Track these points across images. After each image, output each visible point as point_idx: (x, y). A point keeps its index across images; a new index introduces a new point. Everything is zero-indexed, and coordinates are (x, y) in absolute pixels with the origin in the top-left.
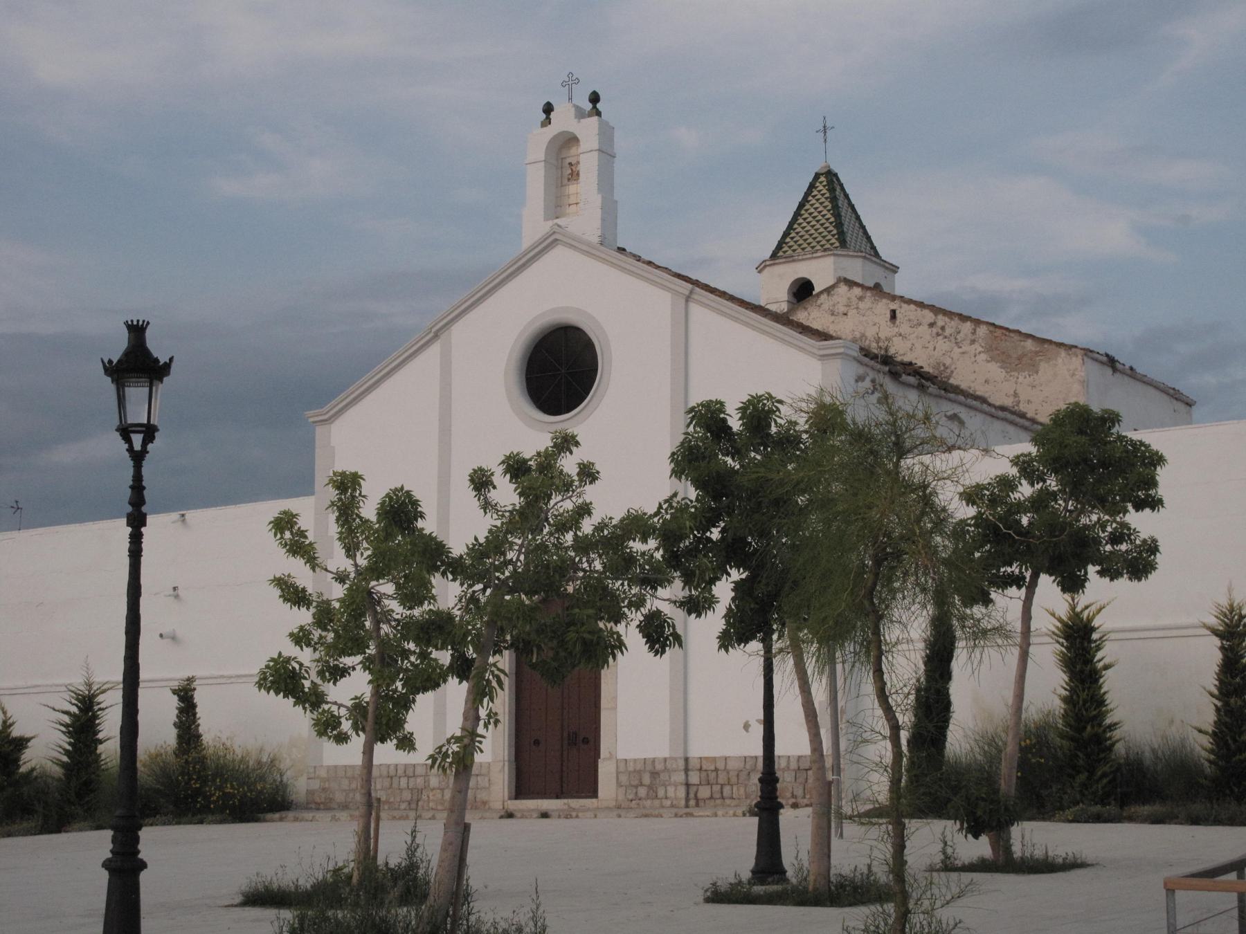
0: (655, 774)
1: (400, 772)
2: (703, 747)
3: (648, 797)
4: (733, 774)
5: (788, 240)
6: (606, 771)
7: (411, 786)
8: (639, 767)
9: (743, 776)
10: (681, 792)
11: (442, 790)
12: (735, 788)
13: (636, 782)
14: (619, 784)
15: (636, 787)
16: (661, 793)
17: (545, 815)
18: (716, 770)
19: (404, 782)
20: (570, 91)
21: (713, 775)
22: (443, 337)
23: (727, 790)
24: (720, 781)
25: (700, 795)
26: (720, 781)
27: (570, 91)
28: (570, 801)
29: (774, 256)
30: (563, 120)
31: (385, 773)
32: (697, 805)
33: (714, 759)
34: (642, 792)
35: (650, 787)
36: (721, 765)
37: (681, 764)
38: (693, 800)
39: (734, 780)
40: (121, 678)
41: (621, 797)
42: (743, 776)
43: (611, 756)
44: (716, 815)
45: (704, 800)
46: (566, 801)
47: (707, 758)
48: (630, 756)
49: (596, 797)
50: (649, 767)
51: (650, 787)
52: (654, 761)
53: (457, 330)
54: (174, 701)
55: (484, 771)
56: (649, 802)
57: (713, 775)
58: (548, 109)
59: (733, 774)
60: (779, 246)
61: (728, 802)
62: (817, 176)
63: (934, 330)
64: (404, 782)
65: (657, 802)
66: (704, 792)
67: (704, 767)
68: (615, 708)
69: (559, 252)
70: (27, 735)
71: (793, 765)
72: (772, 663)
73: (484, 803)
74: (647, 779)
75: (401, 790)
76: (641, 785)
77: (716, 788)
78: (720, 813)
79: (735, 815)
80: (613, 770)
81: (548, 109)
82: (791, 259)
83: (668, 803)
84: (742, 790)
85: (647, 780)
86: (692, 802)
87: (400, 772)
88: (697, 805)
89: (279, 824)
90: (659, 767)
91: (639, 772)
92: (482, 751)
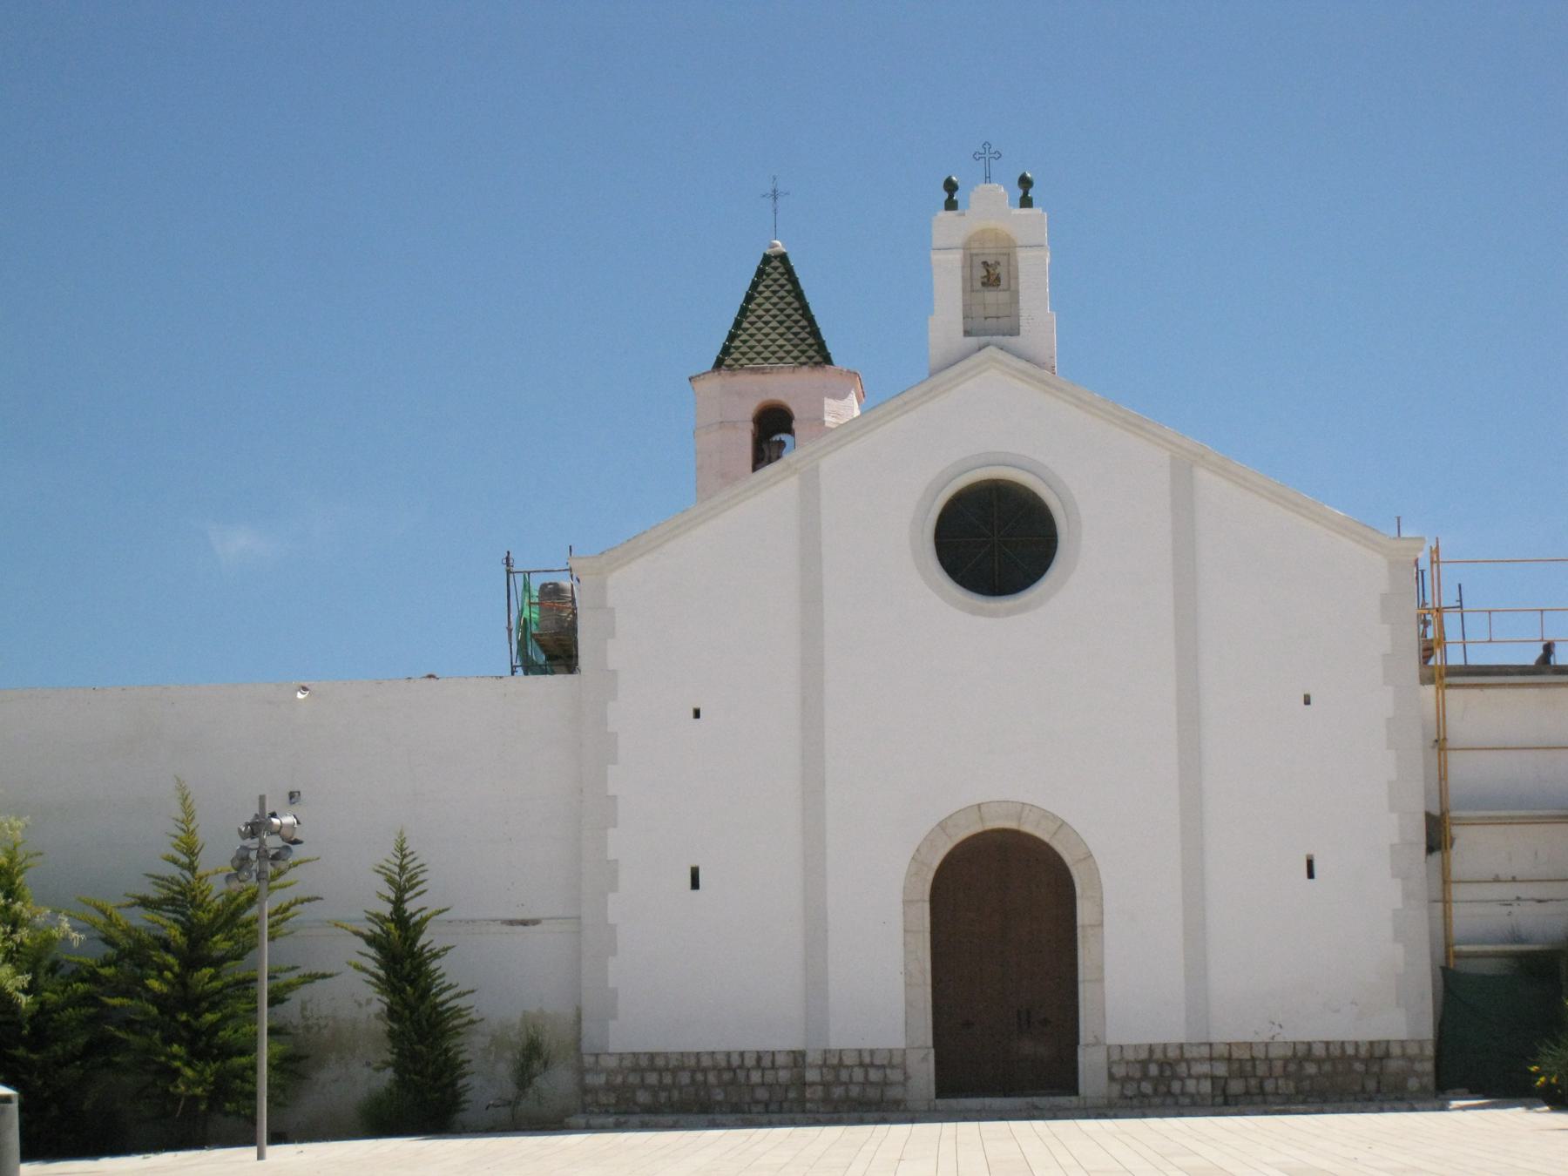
0: (1165, 1064)
4: (1279, 1064)
5: (737, 343)
8: (1144, 1055)
9: (1292, 1067)
12: (1280, 1082)
14: (1112, 1077)
15: (1190, 1076)
18: (1253, 1059)
21: (1248, 1067)
29: (719, 364)
34: (1147, 1087)
43: (1098, 1043)
45: (1236, 1096)
46: (1029, 1099)
47: (1238, 1044)
49: (1076, 1093)
57: (1248, 1067)
60: (726, 351)
61: (1270, 1098)
62: (767, 259)
63: (46, 963)
66: (1236, 1086)
67: (1235, 1055)
68: (1101, 980)
71: (1363, 1051)
72: (645, 1064)
75: (753, 1087)
77: (1253, 1082)
86: (1220, 1100)
87: (766, 1062)
92: (260, 1156)
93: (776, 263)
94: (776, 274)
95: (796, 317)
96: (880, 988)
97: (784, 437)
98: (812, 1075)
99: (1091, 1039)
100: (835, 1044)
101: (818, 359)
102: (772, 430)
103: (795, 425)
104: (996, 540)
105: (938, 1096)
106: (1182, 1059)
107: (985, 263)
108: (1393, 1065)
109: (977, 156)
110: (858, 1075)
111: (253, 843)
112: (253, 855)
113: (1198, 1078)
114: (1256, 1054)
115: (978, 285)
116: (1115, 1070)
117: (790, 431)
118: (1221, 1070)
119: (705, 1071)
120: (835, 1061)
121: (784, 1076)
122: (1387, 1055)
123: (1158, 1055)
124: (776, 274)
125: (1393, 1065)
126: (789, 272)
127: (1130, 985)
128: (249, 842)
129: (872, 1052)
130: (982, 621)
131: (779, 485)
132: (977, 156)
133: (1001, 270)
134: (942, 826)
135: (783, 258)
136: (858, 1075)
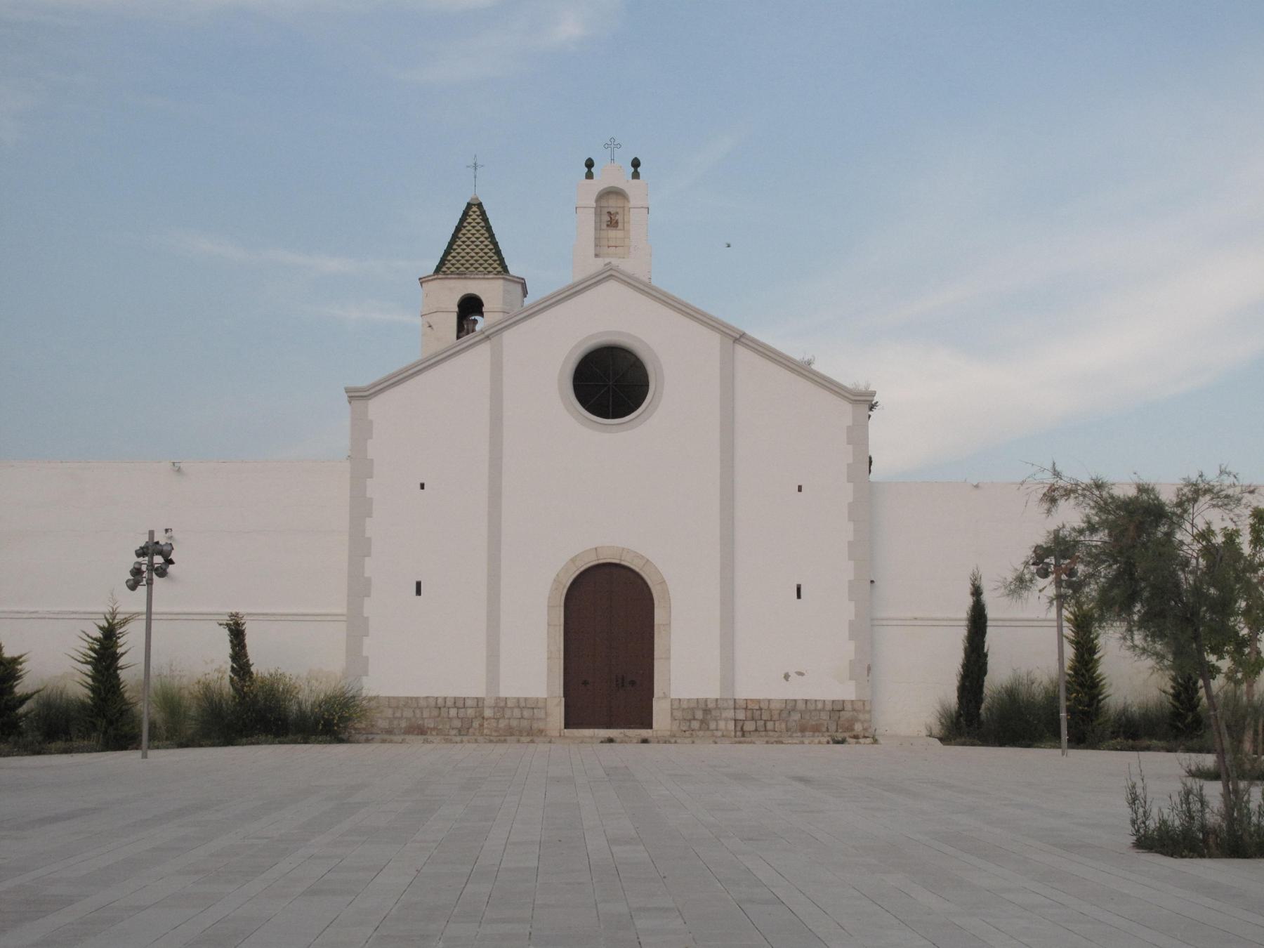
0: (707, 711)
1: (449, 703)
2: (511, 689)
3: (700, 729)
4: (776, 713)
6: (660, 709)
7: (461, 715)
8: (693, 705)
9: (784, 715)
10: (731, 725)
11: (498, 719)
13: (690, 717)
14: (673, 718)
16: (713, 725)
17: (611, 740)
18: (761, 709)
19: (453, 712)
20: (612, 153)
22: (494, 339)
23: (770, 725)
24: (764, 717)
25: (745, 728)
26: (764, 717)
27: (612, 153)
28: (596, 731)
29: (438, 270)
30: (603, 178)
31: (433, 704)
32: (743, 736)
33: (759, 701)
34: (695, 725)
35: (702, 722)
36: (764, 706)
37: (731, 703)
38: (742, 733)
39: (776, 717)
40: (989, 630)
41: (675, 728)
42: (784, 715)
43: (665, 696)
44: (803, 743)
48: (685, 695)
50: (702, 705)
51: (702, 722)
52: (706, 700)
53: (507, 335)
54: (225, 634)
55: (541, 704)
56: (701, 733)
58: (590, 164)
59: (776, 713)
62: (469, 206)
64: (453, 712)
65: (708, 733)
66: (750, 726)
69: (612, 285)
70: (16, 655)
71: (829, 707)
73: (541, 731)
74: (699, 715)
76: (694, 719)
77: (761, 723)
78: (806, 741)
79: (820, 743)
80: (669, 707)
81: (590, 164)
82: (461, 275)
83: (719, 734)
84: (783, 726)
85: (698, 718)
86: (739, 734)
88: (743, 736)
89: (367, 745)
90: (711, 705)
91: (693, 709)
93: (475, 209)
94: (474, 213)
95: (491, 254)
96: (531, 666)
97: (477, 317)
98: (488, 713)
99: (661, 695)
100: (503, 694)
101: (499, 269)
102: (470, 307)
103: (484, 309)
104: (610, 383)
105: (568, 725)
106: (717, 708)
107: (609, 213)
108: (846, 715)
109: (606, 146)
110: (517, 713)
111: (145, 560)
112: (144, 568)
113: (726, 720)
114: (762, 705)
115: (604, 226)
116: (676, 713)
117: (481, 314)
118: (741, 715)
119: (421, 709)
120: (502, 704)
121: (470, 712)
122: (794, 709)
123: (801, 706)
124: (474, 213)
125: (846, 715)
126: (483, 213)
127: (686, 666)
128: (141, 559)
129: (526, 699)
130: (606, 186)
131: (477, 358)
132: (606, 146)
133: (619, 217)
134: (573, 560)
135: (480, 205)
136: (517, 713)
